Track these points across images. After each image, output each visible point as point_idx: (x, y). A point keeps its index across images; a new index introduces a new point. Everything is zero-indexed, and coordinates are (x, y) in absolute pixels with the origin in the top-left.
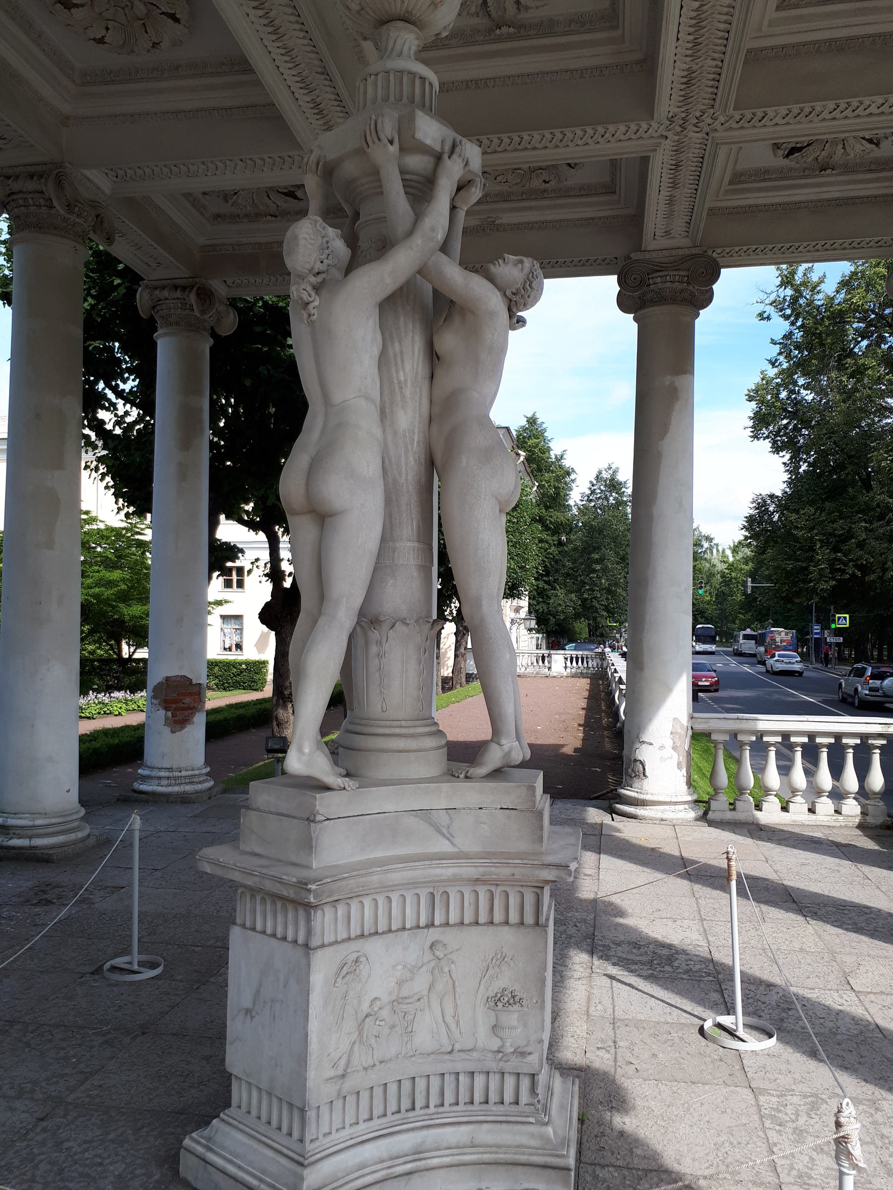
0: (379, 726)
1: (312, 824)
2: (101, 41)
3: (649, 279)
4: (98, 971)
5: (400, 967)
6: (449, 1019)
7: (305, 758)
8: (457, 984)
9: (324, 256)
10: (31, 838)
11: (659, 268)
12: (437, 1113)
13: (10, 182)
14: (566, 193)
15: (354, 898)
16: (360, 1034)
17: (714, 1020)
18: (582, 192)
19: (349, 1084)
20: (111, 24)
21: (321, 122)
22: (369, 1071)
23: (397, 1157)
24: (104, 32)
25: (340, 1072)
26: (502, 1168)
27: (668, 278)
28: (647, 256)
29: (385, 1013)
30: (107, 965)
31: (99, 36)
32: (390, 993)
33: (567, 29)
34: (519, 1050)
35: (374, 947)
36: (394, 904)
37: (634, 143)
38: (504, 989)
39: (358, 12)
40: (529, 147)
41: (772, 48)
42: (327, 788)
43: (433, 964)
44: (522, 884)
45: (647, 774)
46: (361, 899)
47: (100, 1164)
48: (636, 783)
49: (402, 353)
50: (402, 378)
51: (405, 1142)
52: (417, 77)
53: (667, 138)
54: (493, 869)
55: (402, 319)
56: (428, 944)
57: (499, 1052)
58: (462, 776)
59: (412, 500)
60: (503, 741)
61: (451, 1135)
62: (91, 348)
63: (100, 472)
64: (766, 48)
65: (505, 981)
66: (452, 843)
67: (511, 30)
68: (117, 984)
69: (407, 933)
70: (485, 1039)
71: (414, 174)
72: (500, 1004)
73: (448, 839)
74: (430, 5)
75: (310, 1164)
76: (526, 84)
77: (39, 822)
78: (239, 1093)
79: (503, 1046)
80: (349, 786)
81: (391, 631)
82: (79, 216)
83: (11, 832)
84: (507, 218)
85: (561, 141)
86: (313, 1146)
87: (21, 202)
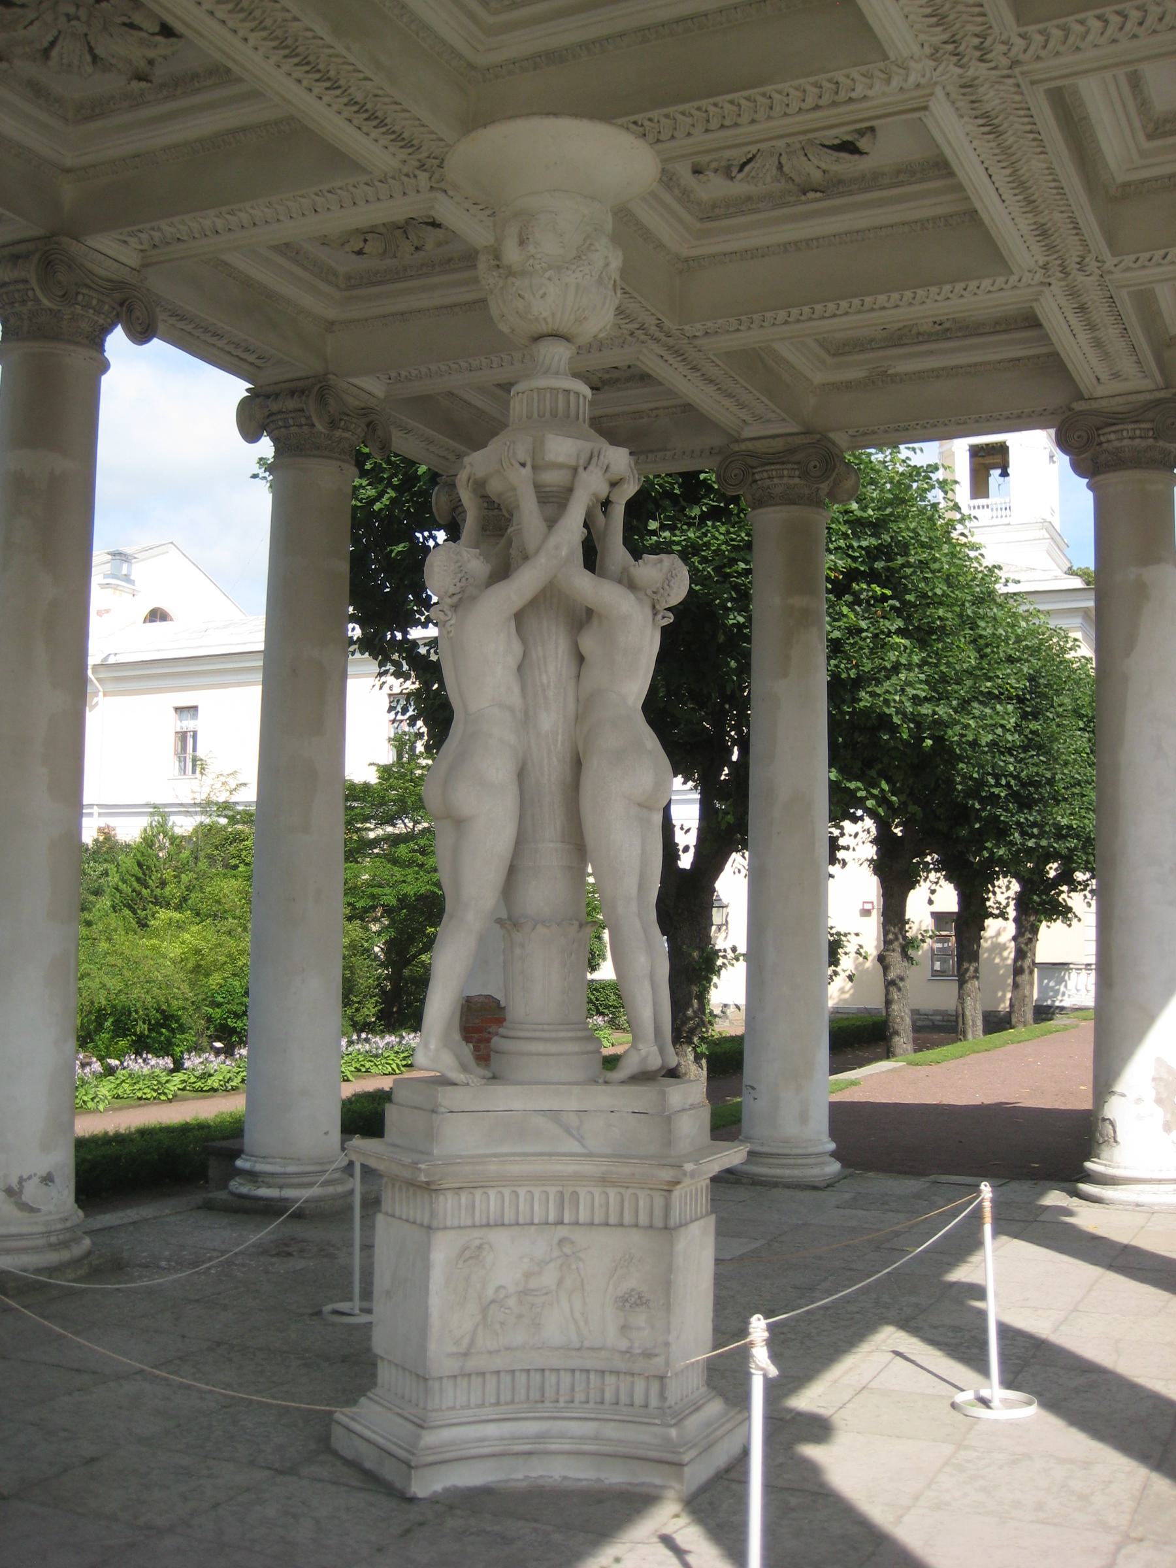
0: (528, 1030)
1: (434, 1115)
2: (360, 253)
3: (1099, 435)
4: (318, 1313)
5: (526, 1260)
9: (457, 580)
10: (281, 1187)
11: (1114, 421)
16: (484, 1317)
17: (977, 1392)
18: (998, 328)
19: (472, 1364)
24: (362, 244)
25: (463, 1349)
27: (1125, 433)
29: (512, 1302)
30: (328, 1308)
31: (356, 249)
35: (499, 1238)
36: (521, 1199)
38: (633, 1290)
41: (1156, 179)
44: (644, 1185)
45: (1118, 1139)
48: (1105, 1153)
50: (545, 681)
51: (532, 1428)
53: (1050, 284)
54: (613, 1168)
58: (601, 1080)
60: (641, 1046)
61: (576, 1428)
62: (393, 555)
63: (408, 714)
64: (1147, 180)
65: (633, 1281)
68: (333, 1325)
69: (533, 1228)
70: (612, 1338)
72: (627, 1305)
73: (578, 1140)
77: (291, 1169)
78: (385, 1373)
79: (631, 1347)
82: (346, 429)
83: (260, 1179)
87: (281, 423)
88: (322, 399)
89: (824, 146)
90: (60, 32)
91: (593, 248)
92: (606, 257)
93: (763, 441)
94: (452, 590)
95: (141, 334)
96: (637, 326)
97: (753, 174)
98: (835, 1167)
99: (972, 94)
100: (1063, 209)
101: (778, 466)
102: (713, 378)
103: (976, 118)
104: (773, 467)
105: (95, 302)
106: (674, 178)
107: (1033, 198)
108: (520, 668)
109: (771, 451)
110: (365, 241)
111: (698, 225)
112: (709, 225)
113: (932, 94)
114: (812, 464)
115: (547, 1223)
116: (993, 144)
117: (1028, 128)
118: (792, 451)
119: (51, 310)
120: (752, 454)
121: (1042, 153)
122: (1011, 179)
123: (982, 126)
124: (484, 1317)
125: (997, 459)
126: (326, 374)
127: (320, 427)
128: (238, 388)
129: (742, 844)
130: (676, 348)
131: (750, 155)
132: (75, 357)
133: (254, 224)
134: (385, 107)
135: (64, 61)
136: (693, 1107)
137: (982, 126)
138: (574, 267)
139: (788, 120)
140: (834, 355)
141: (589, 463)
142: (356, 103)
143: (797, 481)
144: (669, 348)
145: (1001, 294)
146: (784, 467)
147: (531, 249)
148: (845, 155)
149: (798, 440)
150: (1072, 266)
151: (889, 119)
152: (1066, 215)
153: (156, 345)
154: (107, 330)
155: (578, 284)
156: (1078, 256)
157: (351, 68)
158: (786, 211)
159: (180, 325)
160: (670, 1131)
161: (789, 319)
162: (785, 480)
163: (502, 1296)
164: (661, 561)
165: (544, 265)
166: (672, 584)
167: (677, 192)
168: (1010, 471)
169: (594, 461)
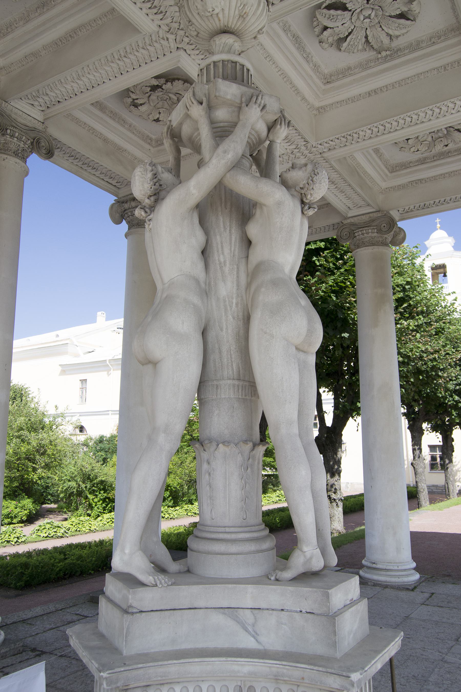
2: (157, 120)
13: (124, 204)
15: (166, 685)
20: (161, 110)
39: (197, 36)
42: (143, 585)
46: (172, 686)
50: (222, 260)
52: (238, 64)
55: (221, 219)
59: (232, 348)
66: (257, 640)
67: (388, 53)
71: (225, 122)
73: (253, 637)
74: (239, 17)
76: (408, 83)
80: (161, 583)
81: (216, 452)
85: (440, 113)
89: (391, 16)
93: (359, 217)
96: (294, 147)
97: (352, 43)
98: (417, 576)
101: (366, 228)
102: (334, 180)
104: (364, 229)
105: (17, 134)
106: (310, 56)
108: (203, 252)
109: (362, 221)
110: (160, 113)
111: (323, 87)
112: (329, 86)
114: (383, 225)
120: (353, 224)
125: (442, 270)
128: (112, 199)
129: (357, 411)
131: (350, 30)
133: (93, 87)
136: (353, 603)
143: (375, 234)
146: (369, 228)
149: (375, 215)
158: (369, 71)
159: (75, 162)
160: (335, 632)
161: (372, 136)
162: (370, 234)
166: (314, 179)
167: (311, 65)
168: (447, 274)
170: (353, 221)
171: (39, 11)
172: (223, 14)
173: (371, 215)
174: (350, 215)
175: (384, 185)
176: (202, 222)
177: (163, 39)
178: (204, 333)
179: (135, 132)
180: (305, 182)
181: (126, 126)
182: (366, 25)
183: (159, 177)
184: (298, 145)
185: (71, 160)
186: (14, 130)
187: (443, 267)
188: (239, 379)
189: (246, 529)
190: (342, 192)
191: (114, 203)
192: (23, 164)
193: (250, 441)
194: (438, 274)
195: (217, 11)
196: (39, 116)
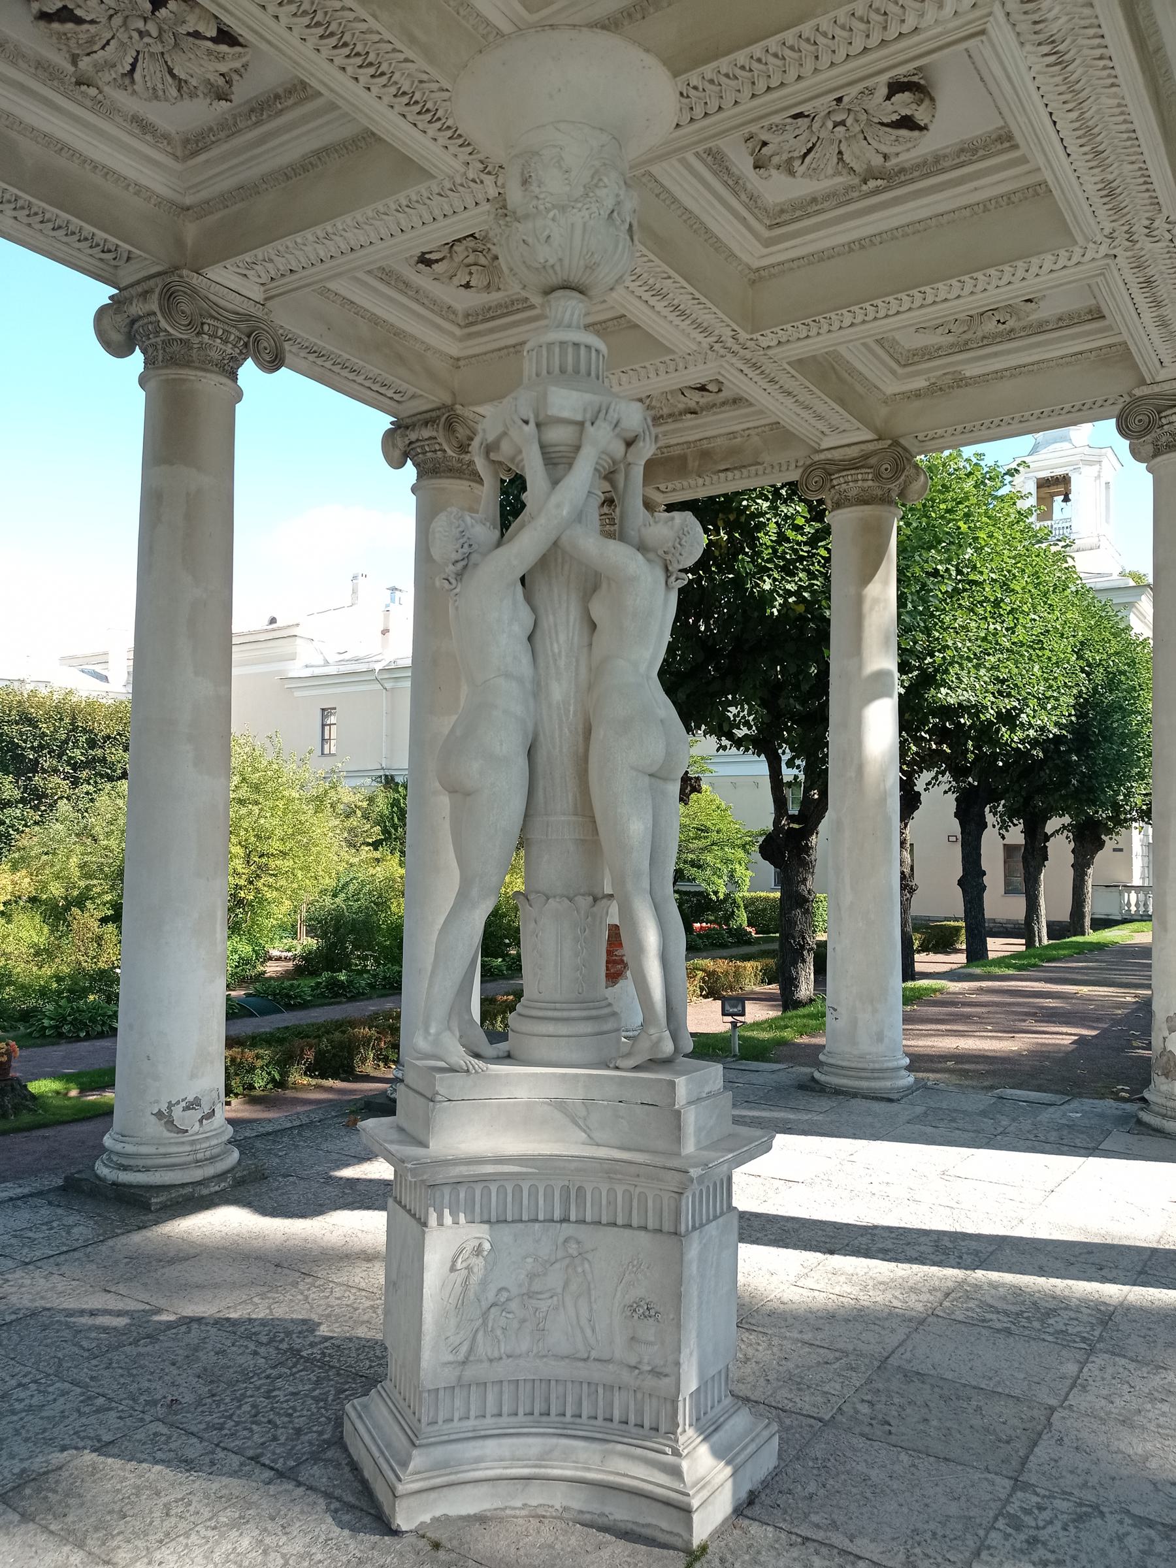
5: (530, 1260)
6: (584, 1322)
7: (431, 1038)
8: (592, 1286)
9: (459, 546)
12: (573, 1423)
14: (1040, 328)
18: (1061, 324)
19: (470, 1373)
21: (688, 322)
22: (495, 1364)
23: (518, 1460)
26: (626, 1495)
28: (1156, 389)
32: (520, 1286)
33: (957, 161)
34: (658, 1370)
37: (1072, 270)
38: (641, 1299)
40: (938, 299)
43: (567, 1261)
47: (291, 1415)
49: (556, 626)
50: (556, 650)
56: (561, 1240)
57: (636, 1368)
67: (879, 182)
72: (636, 1316)
73: (585, 1131)
75: (420, 1446)
79: (640, 1362)
84: (970, 371)
86: (430, 1429)
88: (450, 427)
89: (882, 124)
90: (138, 52)
91: (601, 184)
92: (618, 195)
94: (455, 556)
95: (272, 363)
96: (715, 339)
97: (813, 166)
99: (1035, 12)
100: (1133, 158)
101: (853, 472)
102: (791, 390)
103: (1040, 44)
105: (220, 332)
107: (1100, 148)
108: (530, 638)
110: (471, 274)
113: (990, 14)
115: (552, 1221)
116: (1059, 79)
117: (1098, 52)
118: (866, 456)
119: (181, 340)
120: (831, 462)
121: (1113, 85)
122: (1077, 125)
123: (1046, 55)
124: (485, 1324)
126: (453, 405)
127: (450, 452)
128: (384, 422)
130: (754, 361)
132: (210, 383)
134: (433, 95)
135: (149, 84)
137: (1046, 55)
138: (579, 205)
139: (835, 71)
140: (905, 366)
141: (597, 418)
142: (404, 93)
143: (870, 483)
144: (747, 361)
145: (1064, 272)
147: (534, 188)
148: (904, 132)
149: (871, 447)
150: (1139, 230)
151: (946, 51)
152: (1136, 166)
153: (284, 373)
154: (237, 362)
155: (585, 224)
156: (1148, 219)
157: (389, 47)
159: (319, 361)
163: (502, 1300)
164: (673, 519)
165: (548, 205)
166: (683, 542)
167: (743, 197)
169: (602, 415)
170: (829, 456)
171: (254, 118)
172: (562, 266)
173: (863, 447)
174: (824, 445)
175: (892, 387)
176: (529, 599)
177: (474, 181)
178: (531, 753)
179: (426, 301)
180: (670, 544)
181: (410, 293)
182: (840, 136)
183: (467, 535)
184: (720, 336)
185: (312, 357)
186: (215, 323)
187: (1065, 480)
188: (576, 814)
189: (575, 1006)
190: (807, 408)
191: (390, 430)
192: (229, 382)
193: (590, 895)
194: (1053, 495)
195: (551, 261)
196: (257, 294)
